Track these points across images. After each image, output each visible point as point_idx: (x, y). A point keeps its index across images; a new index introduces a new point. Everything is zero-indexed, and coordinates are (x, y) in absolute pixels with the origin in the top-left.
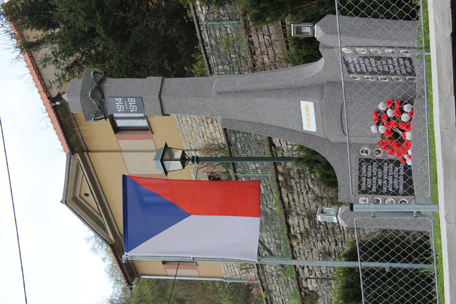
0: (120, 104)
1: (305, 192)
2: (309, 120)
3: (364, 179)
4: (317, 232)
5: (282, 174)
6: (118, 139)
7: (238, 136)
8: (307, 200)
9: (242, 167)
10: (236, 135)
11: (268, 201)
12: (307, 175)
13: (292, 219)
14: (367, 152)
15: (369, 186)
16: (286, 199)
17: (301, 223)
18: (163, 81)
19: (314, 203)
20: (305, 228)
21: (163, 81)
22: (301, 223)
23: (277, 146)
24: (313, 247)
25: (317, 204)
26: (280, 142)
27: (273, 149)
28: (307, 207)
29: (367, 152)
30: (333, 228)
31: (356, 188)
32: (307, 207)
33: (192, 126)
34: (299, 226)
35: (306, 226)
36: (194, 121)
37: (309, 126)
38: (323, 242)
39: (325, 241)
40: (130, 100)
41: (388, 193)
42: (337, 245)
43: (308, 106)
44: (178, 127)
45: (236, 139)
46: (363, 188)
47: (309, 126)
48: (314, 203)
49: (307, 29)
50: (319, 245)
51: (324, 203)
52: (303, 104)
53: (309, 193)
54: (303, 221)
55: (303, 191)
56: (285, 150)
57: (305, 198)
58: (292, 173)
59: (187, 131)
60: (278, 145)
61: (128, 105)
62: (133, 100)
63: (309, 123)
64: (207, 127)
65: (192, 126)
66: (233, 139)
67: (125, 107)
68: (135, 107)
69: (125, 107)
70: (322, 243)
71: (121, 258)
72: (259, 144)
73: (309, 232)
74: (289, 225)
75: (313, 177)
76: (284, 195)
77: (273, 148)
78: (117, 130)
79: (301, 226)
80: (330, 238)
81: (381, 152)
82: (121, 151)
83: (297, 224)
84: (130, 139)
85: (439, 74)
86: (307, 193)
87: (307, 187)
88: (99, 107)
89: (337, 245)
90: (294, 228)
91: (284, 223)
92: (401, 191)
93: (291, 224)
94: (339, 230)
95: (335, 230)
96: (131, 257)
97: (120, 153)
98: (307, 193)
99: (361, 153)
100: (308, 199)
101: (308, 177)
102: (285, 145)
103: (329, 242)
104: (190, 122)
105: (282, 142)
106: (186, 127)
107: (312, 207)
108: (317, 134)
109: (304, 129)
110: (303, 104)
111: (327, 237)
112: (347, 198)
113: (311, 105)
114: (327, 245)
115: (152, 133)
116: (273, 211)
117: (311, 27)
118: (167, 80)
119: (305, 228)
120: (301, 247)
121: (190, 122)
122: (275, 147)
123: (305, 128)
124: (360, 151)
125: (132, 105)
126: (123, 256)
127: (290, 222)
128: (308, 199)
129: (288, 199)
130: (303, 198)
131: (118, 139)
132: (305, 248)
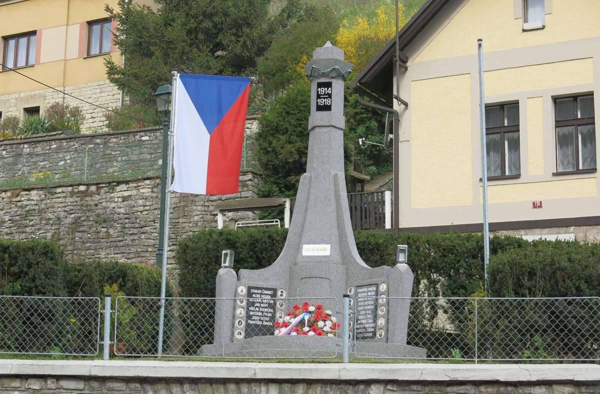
0: (325, 91)
1: (66, 209)
2: (313, 250)
3: (260, 292)
4: (21, 216)
5: (87, 190)
6: (81, 24)
7: (101, 146)
8: (57, 211)
9: (67, 146)
10: (102, 144)
11: (29, 168)
12: (85, 213)
13: (37, 194)
14: (281, 295)
15: (254, 296)
16: (59, 190)
17: (33, 203)
18: (341, 129)
19: (54, 217)
20: (27, 206)
21: (341, 129)
22: (33, 203)
23: (118, 188)
24: (4, 212)
25: (53, 220)
26: (121, 191)
27: (114, 184)
28: (50, 209)
29: (281, 295)
30: (26, 232)
31: (251, 285)
32: (50, 209)
33: (90, 98)
34: (28, 200)
35: (29, 207)
36: (95, 100)
37: (308, 250)
38: (10, 222)
39: (11, 223)
40: (329, 100)
41: (248, 311)
42: (7, 234)
43: (325, 250)
44: (89, 84)
45: (98, 144)
46: (253, 291)
47: (308, 250)
48: (54, 217)
49: (402, 257)
50: (7, 218)
51: (55, 226)
52: (328, 247)
53: (66, 214)
54: (34, 204)
55: (68, 207)
56: (112, 195)
57: (59, 209)
58: (87, 199)
59: (85, 92)
60: (118, 188)
61: (324, 98)
62: (329, 103)
63: (309, 250)
64: (87, 112)
65: (90, 98)
66: (98, 141)
67: (322, 95)
68: (322, 103)
69: (322, 95)
70: (9, 220)
71: (175, 70)
72: (92, 165)
73: (23, 208)
74: (30, 191)
75: (83, 218)
76: (64, 189)
77: (116, 184)
78: (90, 23)
79: (29, 202)
80: (15, 228)
81: (282, 307)
82: (67, 25)
83: (32, 198)
84: (80, 36)
85: (467, 370)
86: (65, 211)
87: (72, 212)
88: (324, 73)
89: (7, 234)
90: (26, 194)
91: (33, 186)
92: (250, 322)
93: (31, 192)
94: (23, 238)
95: (24, 235)
96: (176, 79)
97: (66, 23)
98: (65, 211)
99: (280, 290)
100: (58, 212)
101: (83, 214)
102: (118, 196)
103: (11, 227)
104: (94, 96)
105: (121, 193)
106: (90, 92)
107: (50, 214)
108: (300, 256)
109: (304, 245)
110: (328, 247)
111: (15, 226)
112: (244, 277)
113: (328, 253)
114: (6, 225)
115: (84, 58)
116: (18, 171)
117: (405, 261)
118: (342, 133)
119: (27, 206)
120: (5, 199)
121: (94, 96)
122: (116, 186)
123: (305, 246)
124: (283, 291)
125: (325, 102)
126: (176, 72)
127: (34, 192)
128: (58, 212)
129: (60, 193)
130: (60, 207)
131: (81, 24)
132: (4, 203)
